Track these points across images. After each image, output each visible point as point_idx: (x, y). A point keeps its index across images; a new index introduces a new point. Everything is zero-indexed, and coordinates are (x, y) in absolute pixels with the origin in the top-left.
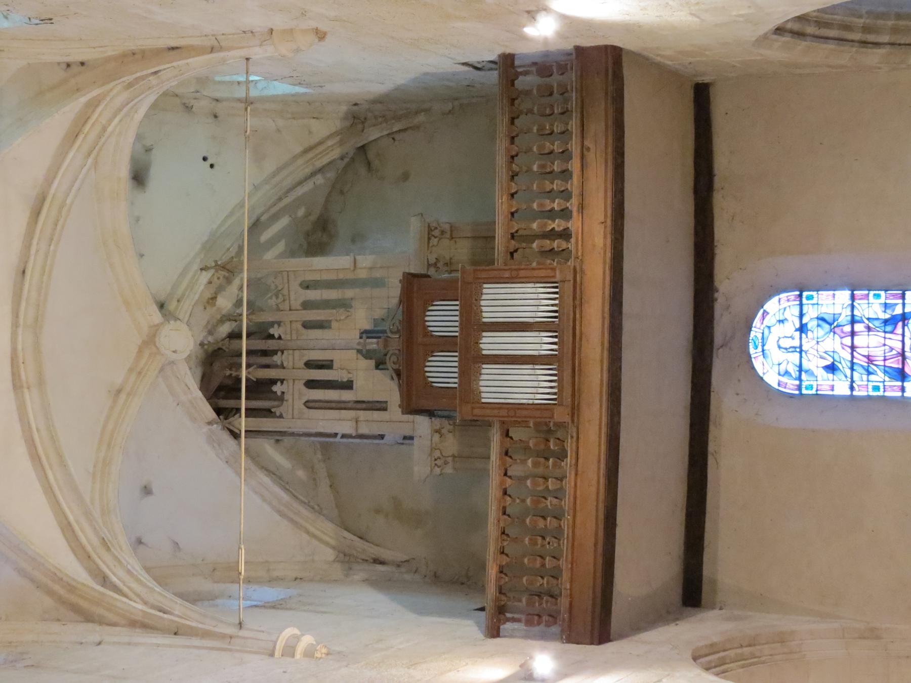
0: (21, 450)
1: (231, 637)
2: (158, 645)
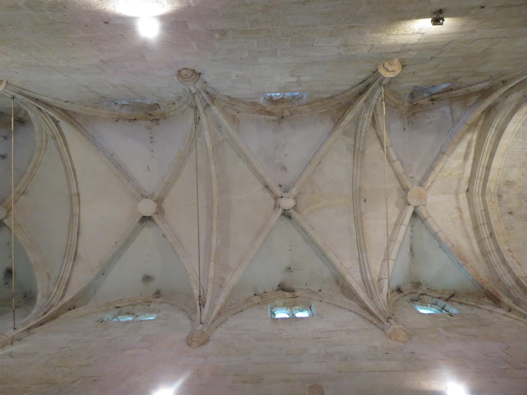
0: (78, 173)
1: (19, 93)
2: (46, 96)
